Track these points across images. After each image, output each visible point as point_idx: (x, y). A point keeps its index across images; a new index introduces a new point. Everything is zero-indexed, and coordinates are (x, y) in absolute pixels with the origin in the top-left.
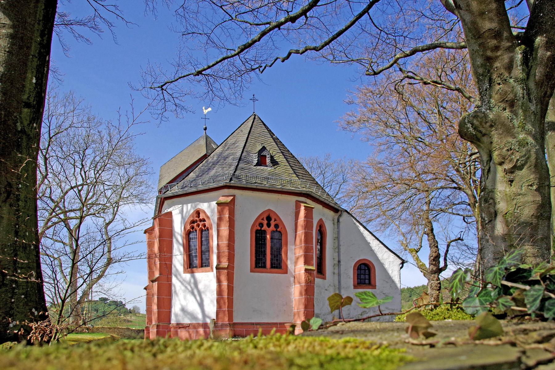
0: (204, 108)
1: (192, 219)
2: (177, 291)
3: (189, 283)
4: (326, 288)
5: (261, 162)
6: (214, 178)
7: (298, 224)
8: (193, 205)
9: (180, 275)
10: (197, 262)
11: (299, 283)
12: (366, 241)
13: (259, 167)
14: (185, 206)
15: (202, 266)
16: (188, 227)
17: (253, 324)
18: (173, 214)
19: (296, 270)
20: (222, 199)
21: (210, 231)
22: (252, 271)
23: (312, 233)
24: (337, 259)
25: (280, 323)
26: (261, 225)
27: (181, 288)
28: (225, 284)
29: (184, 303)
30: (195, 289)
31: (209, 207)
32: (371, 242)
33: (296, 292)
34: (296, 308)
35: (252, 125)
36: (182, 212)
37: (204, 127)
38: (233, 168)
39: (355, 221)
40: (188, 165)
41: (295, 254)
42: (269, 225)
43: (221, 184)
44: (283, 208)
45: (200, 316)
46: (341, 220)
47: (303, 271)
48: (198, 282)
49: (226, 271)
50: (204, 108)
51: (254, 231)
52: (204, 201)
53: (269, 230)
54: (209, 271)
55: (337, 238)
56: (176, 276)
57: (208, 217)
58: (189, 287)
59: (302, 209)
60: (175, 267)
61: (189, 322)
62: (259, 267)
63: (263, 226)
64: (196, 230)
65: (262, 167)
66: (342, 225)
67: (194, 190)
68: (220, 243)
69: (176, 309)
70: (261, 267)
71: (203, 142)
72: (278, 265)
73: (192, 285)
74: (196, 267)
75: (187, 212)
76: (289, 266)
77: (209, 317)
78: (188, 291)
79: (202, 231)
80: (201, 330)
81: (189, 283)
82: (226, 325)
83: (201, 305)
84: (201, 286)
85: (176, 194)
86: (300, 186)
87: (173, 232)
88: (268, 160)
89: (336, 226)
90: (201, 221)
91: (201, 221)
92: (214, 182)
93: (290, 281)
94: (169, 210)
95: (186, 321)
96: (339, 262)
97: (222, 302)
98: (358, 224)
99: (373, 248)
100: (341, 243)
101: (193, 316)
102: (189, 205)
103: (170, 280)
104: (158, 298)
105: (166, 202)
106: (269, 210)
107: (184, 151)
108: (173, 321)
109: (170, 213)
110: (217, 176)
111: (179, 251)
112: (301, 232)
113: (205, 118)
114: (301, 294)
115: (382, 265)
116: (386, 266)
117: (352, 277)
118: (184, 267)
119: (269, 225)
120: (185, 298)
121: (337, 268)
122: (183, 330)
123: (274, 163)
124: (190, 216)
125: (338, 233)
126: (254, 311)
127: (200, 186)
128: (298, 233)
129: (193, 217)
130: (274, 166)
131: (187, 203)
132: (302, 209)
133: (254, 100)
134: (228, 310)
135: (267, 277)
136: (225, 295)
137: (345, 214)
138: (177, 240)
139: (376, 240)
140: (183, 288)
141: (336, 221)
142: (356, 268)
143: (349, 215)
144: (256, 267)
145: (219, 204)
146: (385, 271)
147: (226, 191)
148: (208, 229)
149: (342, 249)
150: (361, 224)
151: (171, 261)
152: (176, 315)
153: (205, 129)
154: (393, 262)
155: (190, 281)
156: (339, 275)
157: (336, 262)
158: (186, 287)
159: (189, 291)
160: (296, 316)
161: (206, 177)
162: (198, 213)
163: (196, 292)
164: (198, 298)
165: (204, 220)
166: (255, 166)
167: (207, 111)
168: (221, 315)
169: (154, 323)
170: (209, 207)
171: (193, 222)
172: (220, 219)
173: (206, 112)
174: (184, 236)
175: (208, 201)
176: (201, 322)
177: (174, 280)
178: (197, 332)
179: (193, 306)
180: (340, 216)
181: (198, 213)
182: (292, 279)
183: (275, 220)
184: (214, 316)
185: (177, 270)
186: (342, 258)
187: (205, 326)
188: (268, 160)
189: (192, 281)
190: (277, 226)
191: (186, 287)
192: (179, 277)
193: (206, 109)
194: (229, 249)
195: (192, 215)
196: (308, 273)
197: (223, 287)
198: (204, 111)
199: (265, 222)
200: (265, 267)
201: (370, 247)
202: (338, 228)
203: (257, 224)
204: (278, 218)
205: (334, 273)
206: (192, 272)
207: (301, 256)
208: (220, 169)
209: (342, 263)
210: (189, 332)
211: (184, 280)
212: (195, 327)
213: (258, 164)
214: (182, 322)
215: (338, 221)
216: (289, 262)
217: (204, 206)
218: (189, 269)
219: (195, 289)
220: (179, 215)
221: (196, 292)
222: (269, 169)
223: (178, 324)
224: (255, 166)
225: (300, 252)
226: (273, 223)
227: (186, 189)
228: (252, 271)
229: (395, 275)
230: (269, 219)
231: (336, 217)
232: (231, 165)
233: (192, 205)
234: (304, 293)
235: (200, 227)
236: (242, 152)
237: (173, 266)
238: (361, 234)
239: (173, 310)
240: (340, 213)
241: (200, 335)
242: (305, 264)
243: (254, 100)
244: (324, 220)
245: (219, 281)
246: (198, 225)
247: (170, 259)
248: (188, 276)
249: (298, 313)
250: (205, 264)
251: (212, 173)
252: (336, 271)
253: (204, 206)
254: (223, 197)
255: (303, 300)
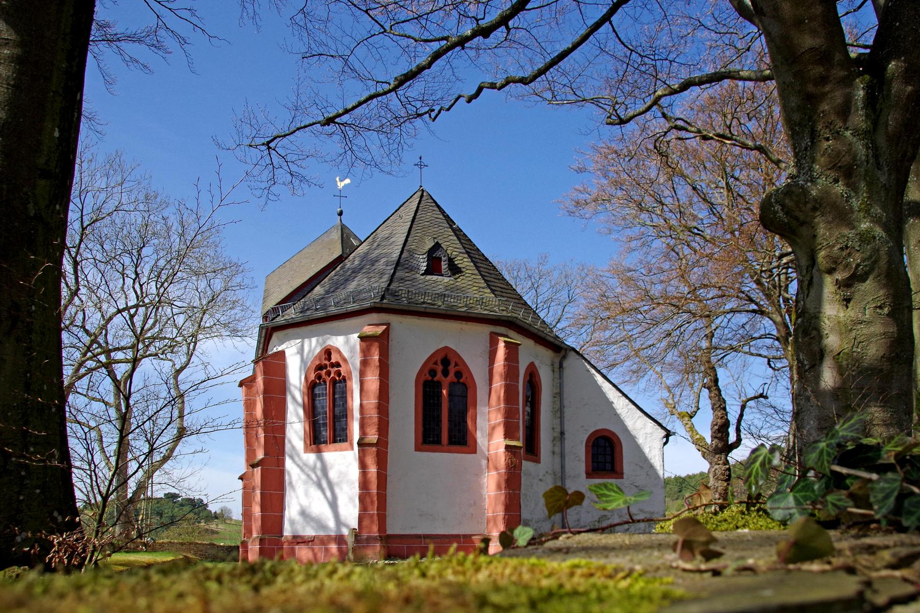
0: (338, 179)
1: (318, 363)
2: (294, 483)
3: (314, 469)
4: (541, 477)
5: (433, 268)
6: (355, 296)
7: (495, 371)
8: (321, 339)
9: (299, 456)
10: (326, 433)
11: (496, 469)
12: (607, 399)
13: (429, 277)
14: (306, 341)
15: (335, 441)
16: (312, 377)
17: (418, 537)
18: (287, 354)
19: (491, 448)
20: (369, 330)
21: (348, 383)
22: (417, 449)
23: (518, 387)
24: (558, 430)
25: (465, 536)
26: (433, 372)
27: (300, 478)
28: (373, 470)
29: (305, 502)
30: (323, 480)
31: (346, 344)
32: (615, 401)
33: (490, 485)
34: (490, 511)
35: (418, 207)
36: (301, 351)
37: (339, 210)
38: (386, 278)
39: (588, 367)
40: (312, 274)
41: (489, 421)
42: (446, 373)
43: (367, 304)
44: (468, 344)
45: (331, 524)
46: (565, 364)
47: (502, 450)
48: (329, 467)
49: (374, 449)
50: (338, 179)
51: (421, 382)
52: (338, 333)
53: (446, 381)
54: (346, 450)
55: (559, 395)
56: (291, 457)
57: (345, 360)
58: (313, 476)
59: (501, 345)
60: (290, 442)
61: (314, 534)
62: (430, 443)
63: (435, 374)
64: (325, 382)
65: (435, 277)
66: (567, 372)
67: (321, 314)
68: (365, 402)
69: (291, 511)
70: (434, 442)
71: (336, 236)
72: (461, 439)
73: (319, 473)
74: (325, 442)
75: (309, 351)
76: (479, 441)
77: (347, 526)
78: (311, 482)
79: (334, 382)
80: (333, 547)
81: (314, 469)
82: (375, 539)
83: (333, 505)
84: (332, 475)
85: (291, 321)
86: (493, 305)
87: (288, 385)
88: (444, 266)
89: (557, 375)
90: (333, 365)
91: (333, 365)
92: (354, 302)
93: (480, 465)
94: (280, 349)
95: (309, 532)
96: (562, 433)
97: (368, 500)
98: (593, 371)
99: (619, 412)
100: (566, 402)
101: (319, 523)
102: (314, 340)
103: (281, 463)
104: (261, 493)
105: (275, 336)
106: (446, 348)
107: (306, 250)
108: (287, 532)
109: (282, 353)
110: (360, 292)
111: (298, 415)
112: (498, 384)
113: (341, 195)
114: (499, 487)
115: (632, 439)
116: (640, 441)
117: (583, 458)
118: (305, 441)
119: (446, 373)
120: (306, 493)
121: (558, 444)
122: (303, 546)
123: (455, 270)
124: (316, 357)
125: (561, 386)
126: (421, 515)
127: (333, 308)
128: (494, 386)
129: (320, 359)
130: (454, 274)
131: (310, 337)
132: (501, 345)
133: (421, 165)
134: (378, 514)
135: (443, 460)
136: (374, 490)
137: (573, 353)
138: (294, 398)
139: (624, 398)
140: (303, 477)
141: (557, 365)
142: (591, 444)
143: (578, 357)
144: (424, 442)
145: (362, 338)
146: (638, 449)
147: (374, 317)
148: (344, 379)
149: (568, 412)
150: (599, 372)
151: (284, 433)
152: (292, 522)
153: (341, 214)
154: (651, 433)
155: (315, 466)
156: (562, 456)
157: (557, 434)
158: (308, 476)
159: (314, 483)
160: (491, 524)
161: (342, 294)
162: (328, 352)
163: (324, 484)
164: (329, 494)
165: (338, 365)
166: (422, 275)
167: (343, 184)
168: (366, 522)
169: (255, 535)
170: (346, 344)
171: (320, 367)
172: (365, 363)
173: (341, 185)
174: (306, 391)
175: (346, 333)
176: (333, 534)
177: (289, 464)
178: (327, 550)
179: (320, 507)
180: (564, 357)
181: (328, 352)
182: (484, 462)
183: (456, 365)
184: (355, 524)
185: (293, 447)
186: (566, 428)
187: (340, 539)
188: (444, 266)
189: (319, 465)
190: (458, 374)
191: (308, 476)
192: (297, 459)
193: (341, 181)
194: (379, 413)
195: (319, 356)
196: (511, 452)
197: (369, 475)
198: (339, 184)
199: (440, 368)
200: (438, 441)
201: (614, 410)
202: (561, 377)
203: (426, 371)
204: (460, 361)
205: (554, 453)
206: (319, 451)
207: (499, 424)
208: (365, 280)
209: (567, 436)
210: (313, 550)
211: (305, 464)
212: (323, 541)
213: (427, 273)
214: (301, 534)
215: (561, 366)
216: (479, 435)
217: (338, 342)
218: (313, 446)
219: (323, 480)
220: (297, 355)
221: (324, 484)
222: (446, 279)
223: (294, 537)
224: (422, 275)
225: (497, 418)
226: (452, 369)
227: (309, 313)
228: (417, 449)
229: (655, 456)
230: (446, 362)
231: (557, 361)
232: (382, 274)
233: (318, 340)
234: (503, 486)
235: (332, 375)
236: (402, 252)
237: (286, 441)
238: (599, 388)
239: (287, 513)
240: (563, 352)
241: (332, 555)
242: (505, 438)
243: (421, 165)
244: (537, 364)
245: (363, 465)
246: (329, 373)
247: (282, 429)
248: (311, 458)
249: (495, 518)
250: (339, 436)
251: (352, 286)
252: (557, 450)
253: (338, 342)
254: (370, 326)
255: (503, 498)
